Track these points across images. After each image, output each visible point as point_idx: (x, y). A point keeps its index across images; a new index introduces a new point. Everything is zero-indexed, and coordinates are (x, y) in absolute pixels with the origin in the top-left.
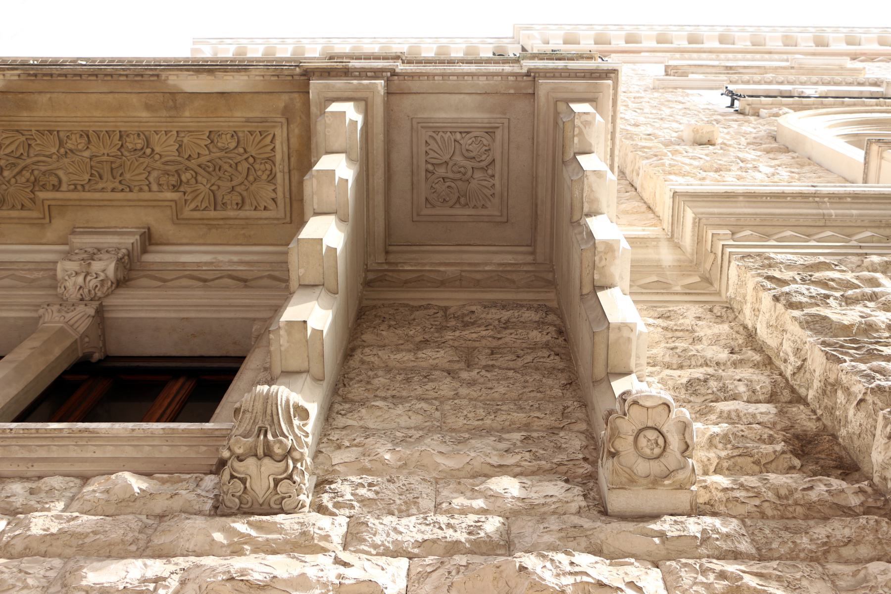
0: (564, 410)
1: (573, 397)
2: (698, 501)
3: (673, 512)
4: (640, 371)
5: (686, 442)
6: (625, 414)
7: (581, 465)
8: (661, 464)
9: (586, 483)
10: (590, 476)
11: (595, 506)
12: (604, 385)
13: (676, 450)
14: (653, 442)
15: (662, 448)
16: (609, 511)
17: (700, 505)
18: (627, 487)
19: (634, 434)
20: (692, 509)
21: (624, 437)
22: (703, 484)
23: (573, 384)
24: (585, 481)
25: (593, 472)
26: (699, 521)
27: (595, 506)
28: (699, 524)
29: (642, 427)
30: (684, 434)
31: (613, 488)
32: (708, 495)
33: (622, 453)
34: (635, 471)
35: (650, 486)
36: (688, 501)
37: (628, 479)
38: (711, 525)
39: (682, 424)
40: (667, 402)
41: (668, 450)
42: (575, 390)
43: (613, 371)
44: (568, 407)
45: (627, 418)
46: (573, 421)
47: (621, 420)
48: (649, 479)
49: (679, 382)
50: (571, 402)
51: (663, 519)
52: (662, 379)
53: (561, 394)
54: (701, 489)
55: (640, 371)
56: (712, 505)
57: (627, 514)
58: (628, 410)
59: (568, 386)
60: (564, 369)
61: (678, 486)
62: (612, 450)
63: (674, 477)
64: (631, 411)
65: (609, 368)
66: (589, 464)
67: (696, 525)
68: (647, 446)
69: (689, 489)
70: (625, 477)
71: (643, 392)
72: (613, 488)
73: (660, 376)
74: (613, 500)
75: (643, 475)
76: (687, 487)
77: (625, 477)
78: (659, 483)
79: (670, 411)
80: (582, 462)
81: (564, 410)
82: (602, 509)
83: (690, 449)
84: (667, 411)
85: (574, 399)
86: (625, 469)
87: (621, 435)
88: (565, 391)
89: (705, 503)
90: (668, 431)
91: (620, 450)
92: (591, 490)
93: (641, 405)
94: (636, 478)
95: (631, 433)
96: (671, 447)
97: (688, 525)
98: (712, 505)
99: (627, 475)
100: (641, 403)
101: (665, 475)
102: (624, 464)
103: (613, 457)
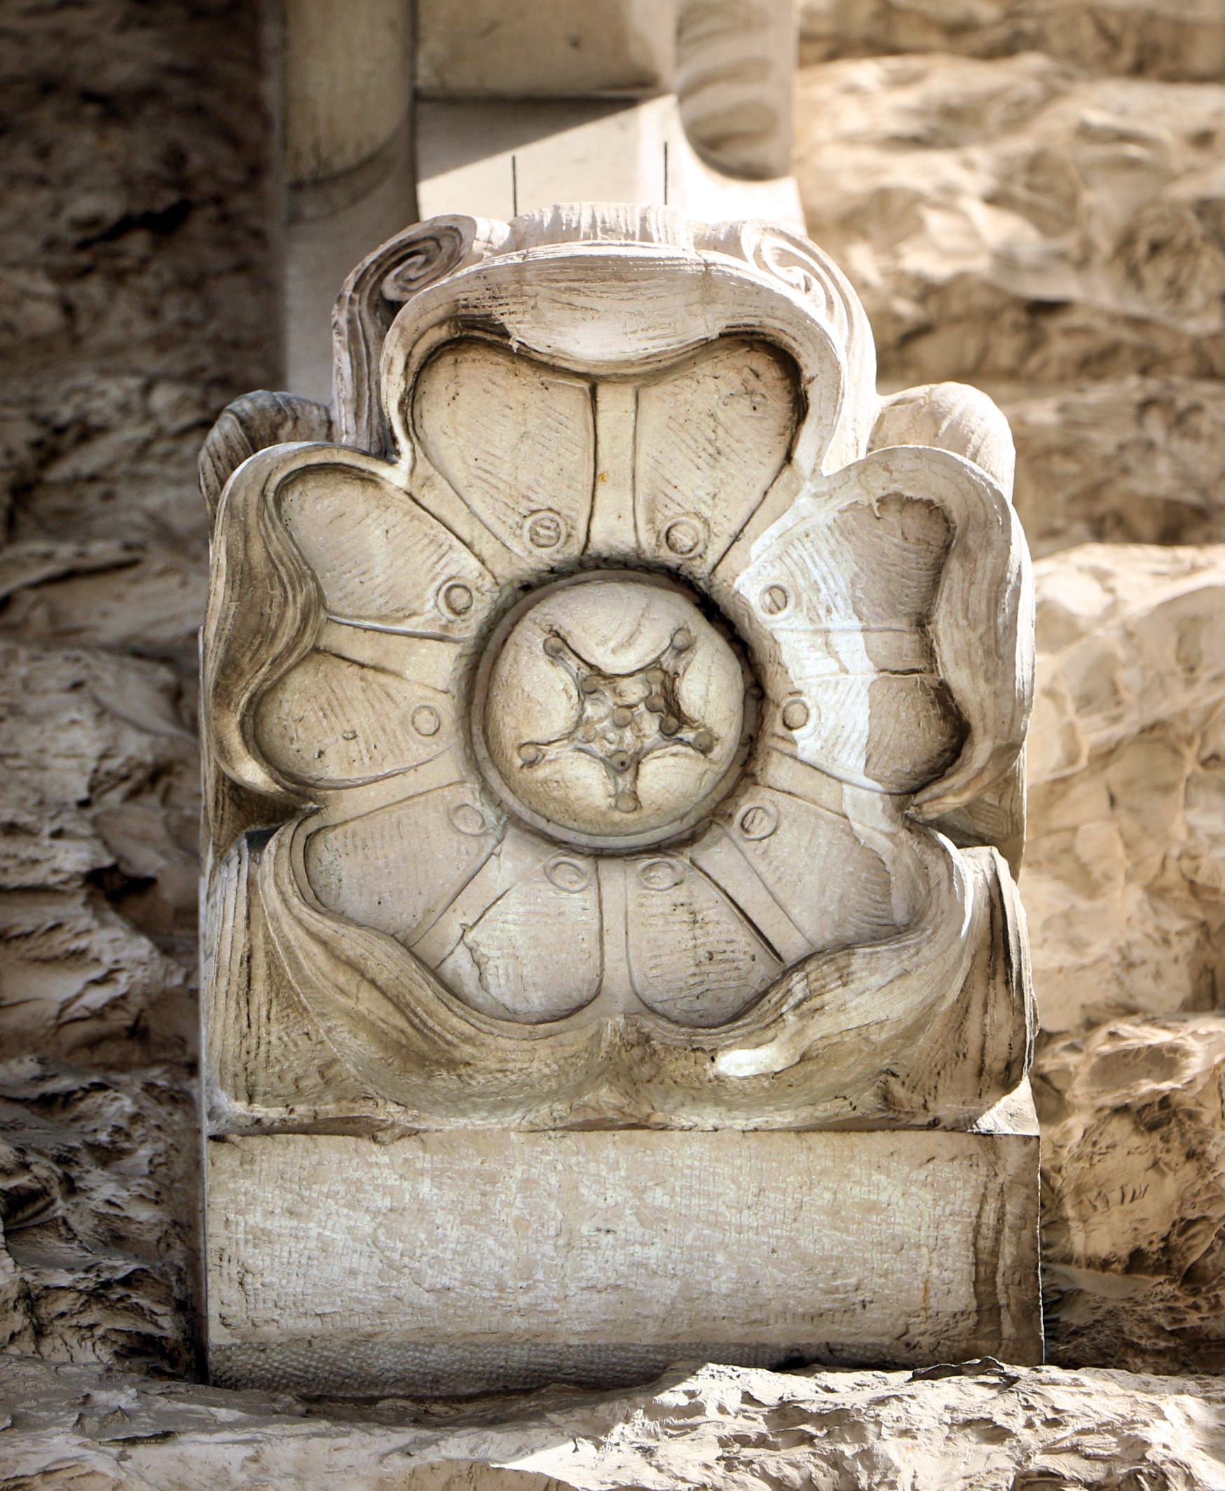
0: (47, 453)
1: (161, 343)
2: (1079, 1241)
3: (810, 1336)
4: (733, 74)
5: (943, 695)
6: (386, 450)
7: (62, 942)
8: (705, 897)
9: (67, 1099)
10: (137, 1032)
11: (97, 1295)
12: (388, 189)
13: (851, 763)
14: (634, 691)
15: (724, 750)
16: (216, 1335)
17: (1083, 1278)
18: (389, 1112)
19: (469, 628)
20: (987, 1309)
21: (363, 649)
22: (1147, 1086)
23: (200, 224)
24: (65, 1083)
25: (161, 1000)
26: (999, 1408)
27: (97, 1295)
28: (994, 1433)
29: (546, 557)
30: (922, 622)
31: (260, 1128)
32: (1170, 1187)
33: (348, 804)
34: (459, 964)
35: (606, 1097)
36: (955, 1232)
37: (379, 1035)
38: (1107, 1444)
39: (914, 522)
40: (772, 324)
41: (778, 771)
42: (194, 284)
43: (464, 78)
44: (87, 432)
45: (395, 476)
46: (103, 550)
47: (347, 496)
48: (574, 1036)
49: (1185, 190)
50: (116, 390)
51: (673, 1397)
52: (1035, 163)
53: (45, 317)
54: (1120, 1129)
55: (733, 74)
56: (1192, 1278)
57: (385, 1361)
58: (410, 400)
59: (137, 243)
60: (150, 93)
61: (868, 1100)
62: (252, 773)
63: (808, 1009)
64: (435, 417)
65: (433, 46)
66: (141, 927)
67: (968, 1444)
68: (579, 728)
69: (962, 1126)
70: (358, 1020)
71: (572, 234)
72: (260, 1128)
73: (1021, 144)
74: (259, 1237)
75: (537, 1001)
76: (947, 1108)
77: (358, 1020)
78: (678, 1066)
79: (799, 408)
80: (75, 912)
81: (47, 453)
82: (167, 1325)
83: (981, 751)
84: (779, 406)
85: (175, 361)
86: (352, 942)
87: (336, 638)
88: (94, 288)
89: (1136, 1261)
90: (779, 596)
91: (332, 770)
92: (107, 1155)
93: (525, 357)
94: (453, 1022)
95: (431, 614)
96: (807, 742)
97: (890, 1448)
98: (1192, 1278)
99: (368, 1003)
100: (523, 331)
101: (732, 1001)
102: (355, 903)
103: (258, 842)
